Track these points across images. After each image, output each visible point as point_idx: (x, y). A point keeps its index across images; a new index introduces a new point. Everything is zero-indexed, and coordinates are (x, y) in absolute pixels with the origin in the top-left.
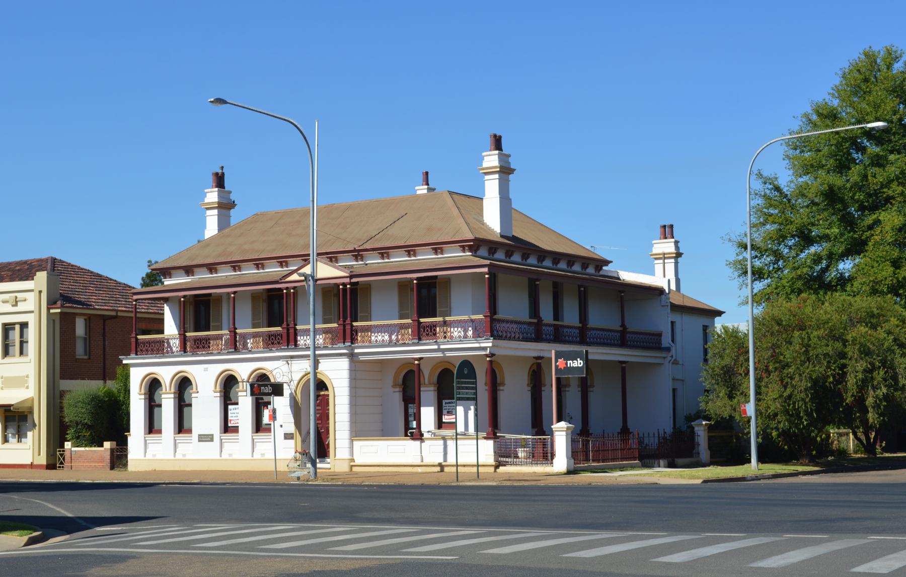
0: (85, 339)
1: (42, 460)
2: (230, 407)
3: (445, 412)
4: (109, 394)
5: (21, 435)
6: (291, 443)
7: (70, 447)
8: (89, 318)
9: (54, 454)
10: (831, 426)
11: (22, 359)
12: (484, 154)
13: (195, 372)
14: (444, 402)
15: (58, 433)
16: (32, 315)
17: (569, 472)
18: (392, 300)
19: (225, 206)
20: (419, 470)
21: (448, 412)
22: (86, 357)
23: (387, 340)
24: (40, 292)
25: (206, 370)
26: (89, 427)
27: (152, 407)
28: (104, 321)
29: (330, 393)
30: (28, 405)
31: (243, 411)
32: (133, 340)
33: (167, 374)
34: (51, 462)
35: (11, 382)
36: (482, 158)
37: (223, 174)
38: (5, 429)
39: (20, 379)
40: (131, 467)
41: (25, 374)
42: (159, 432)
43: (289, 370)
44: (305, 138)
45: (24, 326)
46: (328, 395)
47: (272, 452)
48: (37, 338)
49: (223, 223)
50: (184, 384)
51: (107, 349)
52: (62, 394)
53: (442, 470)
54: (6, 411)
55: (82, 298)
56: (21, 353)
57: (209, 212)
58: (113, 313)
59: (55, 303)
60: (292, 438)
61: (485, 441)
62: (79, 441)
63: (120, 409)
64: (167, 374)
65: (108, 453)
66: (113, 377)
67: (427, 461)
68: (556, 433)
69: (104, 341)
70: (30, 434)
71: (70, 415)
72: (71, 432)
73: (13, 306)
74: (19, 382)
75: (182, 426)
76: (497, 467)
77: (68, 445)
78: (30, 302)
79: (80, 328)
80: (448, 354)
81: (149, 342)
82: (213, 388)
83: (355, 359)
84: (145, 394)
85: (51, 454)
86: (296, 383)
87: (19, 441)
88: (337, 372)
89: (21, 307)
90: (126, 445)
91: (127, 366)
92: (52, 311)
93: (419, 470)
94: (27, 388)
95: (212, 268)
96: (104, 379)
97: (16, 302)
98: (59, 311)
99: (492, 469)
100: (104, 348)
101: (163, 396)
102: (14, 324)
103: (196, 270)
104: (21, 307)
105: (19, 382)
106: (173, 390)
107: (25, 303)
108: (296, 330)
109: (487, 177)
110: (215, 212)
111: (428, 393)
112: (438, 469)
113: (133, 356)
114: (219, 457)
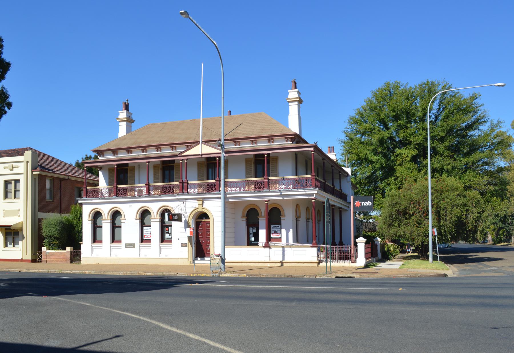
0: (51, 190)
1: (29, 257)
2: (144, 228)
3: (272, 232)
4: (68, 220)
5: (15, 243)
6: (186, 249)
7: (45, 250)
8: (53, 179)
9: (35, 254)
10: (376, 242)
11: (16, 200)
12: (289, 91)
13: (123, 208)
14: (272, 226)
15: (38, 242)
16: (23, 175)
17: (367, 266)
18: (242, 168)
19: (129, 120)
20: (269, 265)
21: (275, 232)
22: (51, 201)
23: (243, 192)
24: (27, 162)
25: (130, 206)
26: (57, 239)
27: (96, 227)
28: (61, 181)
29: (211, 220)
30: (20, 226)
31: (154, 230)
32: (84, 189)
33: (106, 209)
34: (34, 258)
35: (7, 213)
36: (288, 93)
37: (128, 104)
38: (6, 239)
39: (17, 211)
40: (83, 261)
41: (18, 209)
42: (101, 242)
43: (185, 207)
44: (219, 53)
45: (17, 181)
46: (209, 222)
47: (174, 254)
48: (25, 188)
49: (129, 130)
50: (116, 215)
51: (62, 197)
52: (40, 220)
53: (282, 265)
54: (6, 229)
55: (50, 168)
56: (15, 197)
57: (120, 123)
58: (66, 177)
59: (36, 169)
60: (186, 246)
61: (311, 248)
62: (51, 246)
63: (74, 229)
64: (106, 209)
65: (69, 253)
66: (68, 211)
67: (187, 257)
68: (358, 244)
69: (61, 192)
70: (21, 243)
71: (45, 232)
72: (46, 242)
73: (10, 170)
74: (15, 213)
75: (114, 239)
76: (319, 263)
77: (44, 249)
78: (21, 168)
79: (48, 185)
80: (286, 198)
81: (92, 191)
82: (135, 217)
83: (226, 200)
84: (110, 220)
85: (33, 254)
86: (188, 214)
87: (14, 246)
88: (215, 208)
89: (15, 171)
90: (80, 249)
91: (81, 204)
92: (34, 173)
93: (269, 265)
94: (19, 216)
95: (129, 150)
96: (60, 212)
97: (13, 168)
98: (39, 173)
99: (316, 264)
100: (61, 196)
101: (103, 221)
102: (11, 180)
103: (119, 151)
104: (15, 171)
105: (15, 213)
106: (109, 218)
107: (21, 168)
108: (188, 184)
109: (290, 104)
110: (125, 123)
111: (262, 222)
112: (280, 264)
113: (84, 198)
114: (138, 257)
